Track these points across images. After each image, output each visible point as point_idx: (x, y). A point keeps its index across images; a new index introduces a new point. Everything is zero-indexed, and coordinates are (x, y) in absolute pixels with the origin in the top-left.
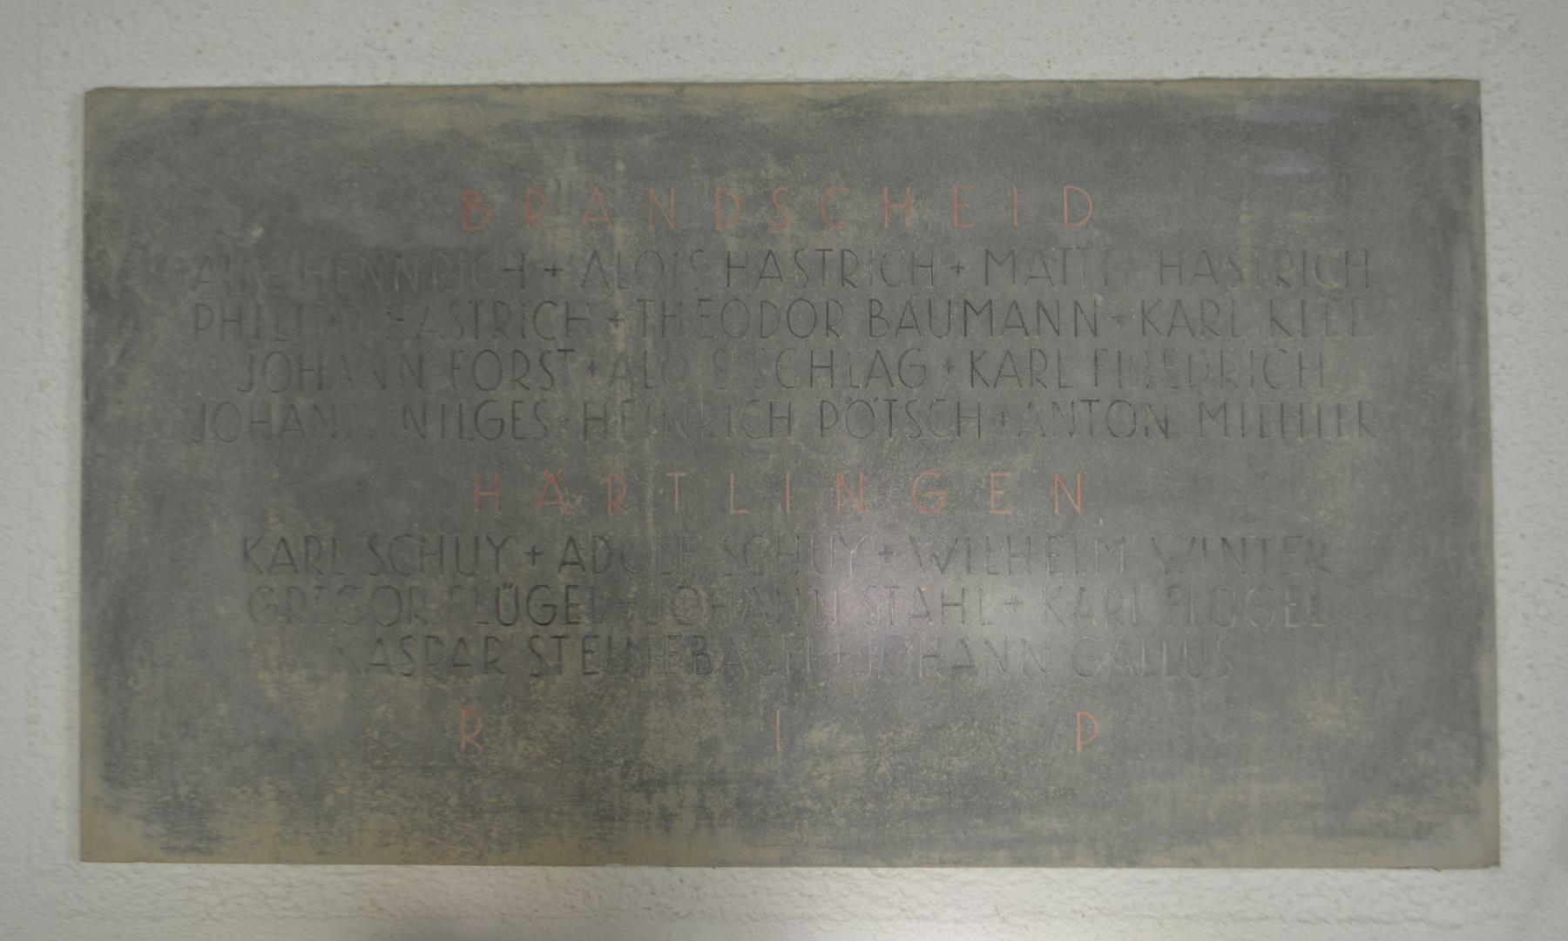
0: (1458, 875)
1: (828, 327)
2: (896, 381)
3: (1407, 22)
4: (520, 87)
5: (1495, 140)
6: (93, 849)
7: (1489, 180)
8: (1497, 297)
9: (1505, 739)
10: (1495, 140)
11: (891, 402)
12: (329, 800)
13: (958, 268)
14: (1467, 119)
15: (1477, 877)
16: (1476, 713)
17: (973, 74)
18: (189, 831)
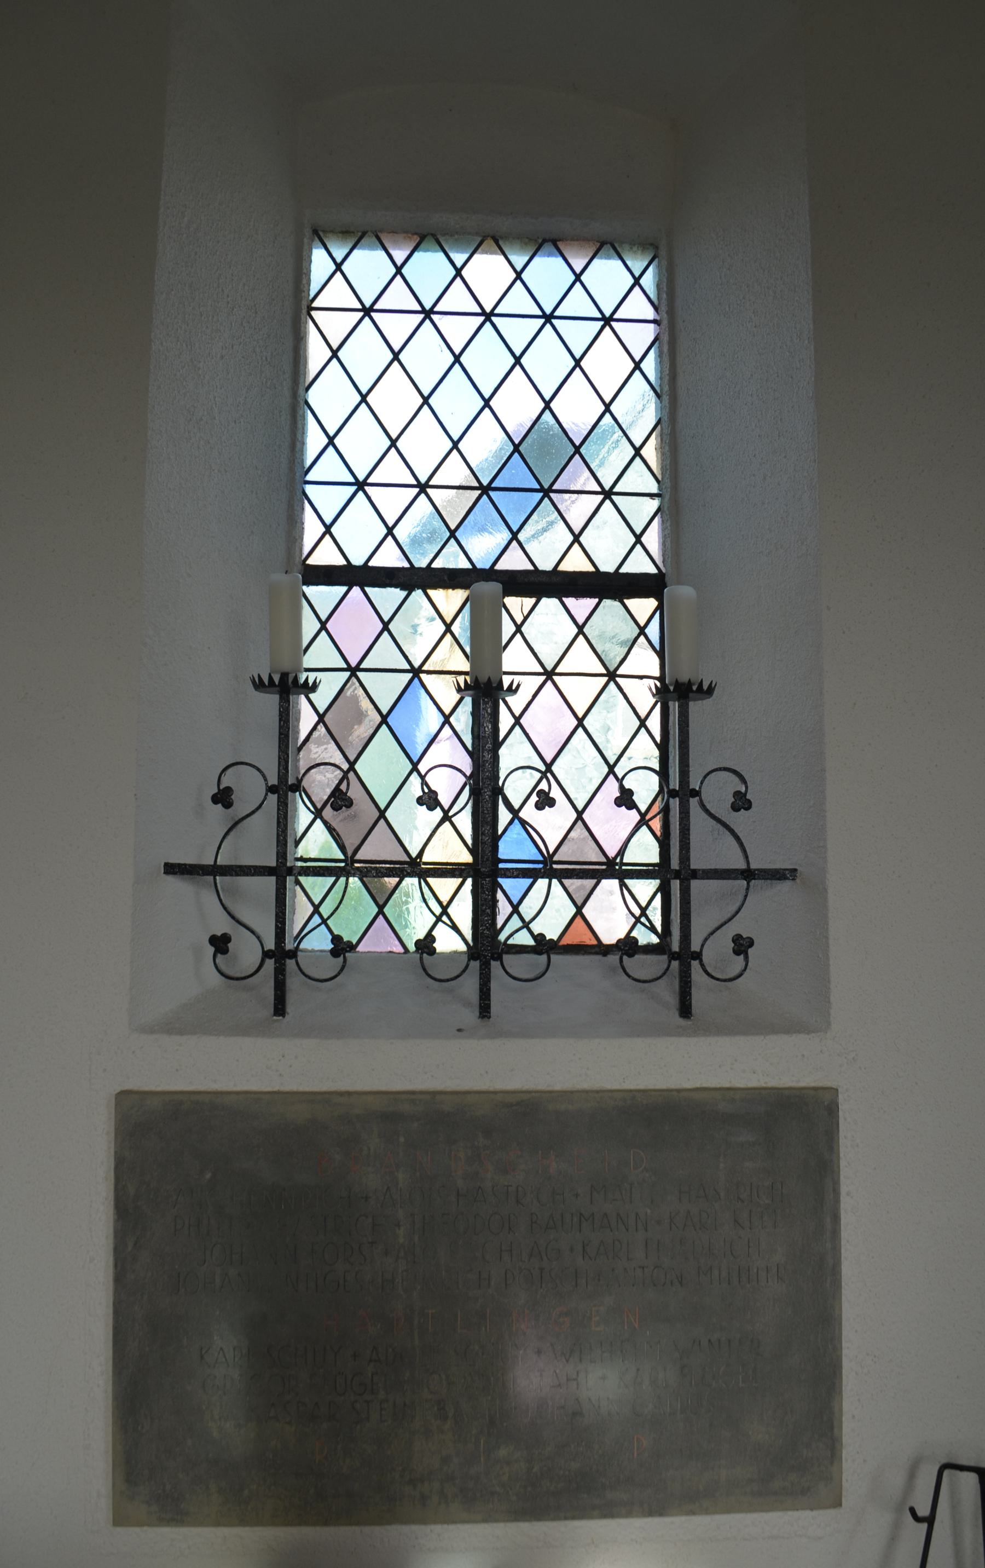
0: (821, 1512)
1: (510, 1229)
2: (545, 1258)
3: (803, 1055)
4: (349, 1093)
5: (845, 1119)
6: (119, 1519)
7: (842, 1141)
8: (846, 1204)
9: (845, 1439)
10: (845, 1119)
11: (542, 1270)
12: (246, 1492)
13: (577, 1195)
14: (832, 1110)
15: (832, 1512)
16: (832, 1428)
17: (585, 1086)
18: (171, 1510)
